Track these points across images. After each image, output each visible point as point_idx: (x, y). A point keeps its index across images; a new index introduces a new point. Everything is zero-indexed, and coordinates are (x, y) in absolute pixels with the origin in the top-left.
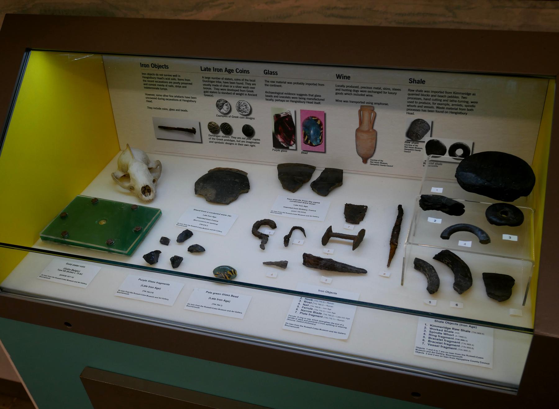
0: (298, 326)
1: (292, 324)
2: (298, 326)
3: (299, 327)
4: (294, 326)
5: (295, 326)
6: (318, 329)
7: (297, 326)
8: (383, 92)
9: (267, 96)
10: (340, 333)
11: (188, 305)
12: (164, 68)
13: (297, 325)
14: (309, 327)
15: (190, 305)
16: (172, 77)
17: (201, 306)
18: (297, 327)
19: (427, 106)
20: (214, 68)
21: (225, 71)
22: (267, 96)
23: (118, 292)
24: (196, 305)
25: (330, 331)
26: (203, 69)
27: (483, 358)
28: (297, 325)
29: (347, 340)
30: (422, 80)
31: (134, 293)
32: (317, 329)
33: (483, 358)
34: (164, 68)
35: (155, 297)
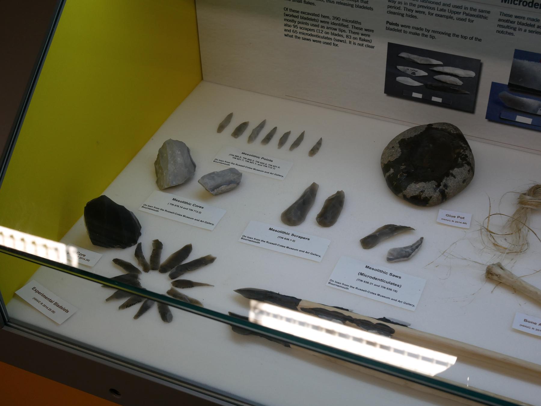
0: (347, 287)
1: (339, 283)
2: (347, 287)
3: (349, 287)
4: (253, 240)
5: (254, 240)
6: (375, 294)
7: (156, 209)
8: (467, 20)
9: (287, 15)
10: (407, 304)
11: (244, 238)
12: (516, 4)
13: (346, 285)
14: (242, 165)
15: (147, 207)
16: (441, 7)
17: (161, 209)
18: (156, 211)
19: (502, 25)
20: (451, 10)
21: (413, 10)
22: (287, 15)
23: (214, 161)
24: (155, 207)
25: (392, 299)
26: (439, 10)
27: (400, 278)
28: (346, 285)
29: (59, 324)
30: (531, 24)
31: (267, 242)
32: (283, 246)
33: (400, 278)
34: (516, 4)
35: (195, 220)
